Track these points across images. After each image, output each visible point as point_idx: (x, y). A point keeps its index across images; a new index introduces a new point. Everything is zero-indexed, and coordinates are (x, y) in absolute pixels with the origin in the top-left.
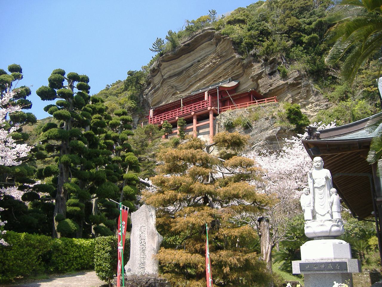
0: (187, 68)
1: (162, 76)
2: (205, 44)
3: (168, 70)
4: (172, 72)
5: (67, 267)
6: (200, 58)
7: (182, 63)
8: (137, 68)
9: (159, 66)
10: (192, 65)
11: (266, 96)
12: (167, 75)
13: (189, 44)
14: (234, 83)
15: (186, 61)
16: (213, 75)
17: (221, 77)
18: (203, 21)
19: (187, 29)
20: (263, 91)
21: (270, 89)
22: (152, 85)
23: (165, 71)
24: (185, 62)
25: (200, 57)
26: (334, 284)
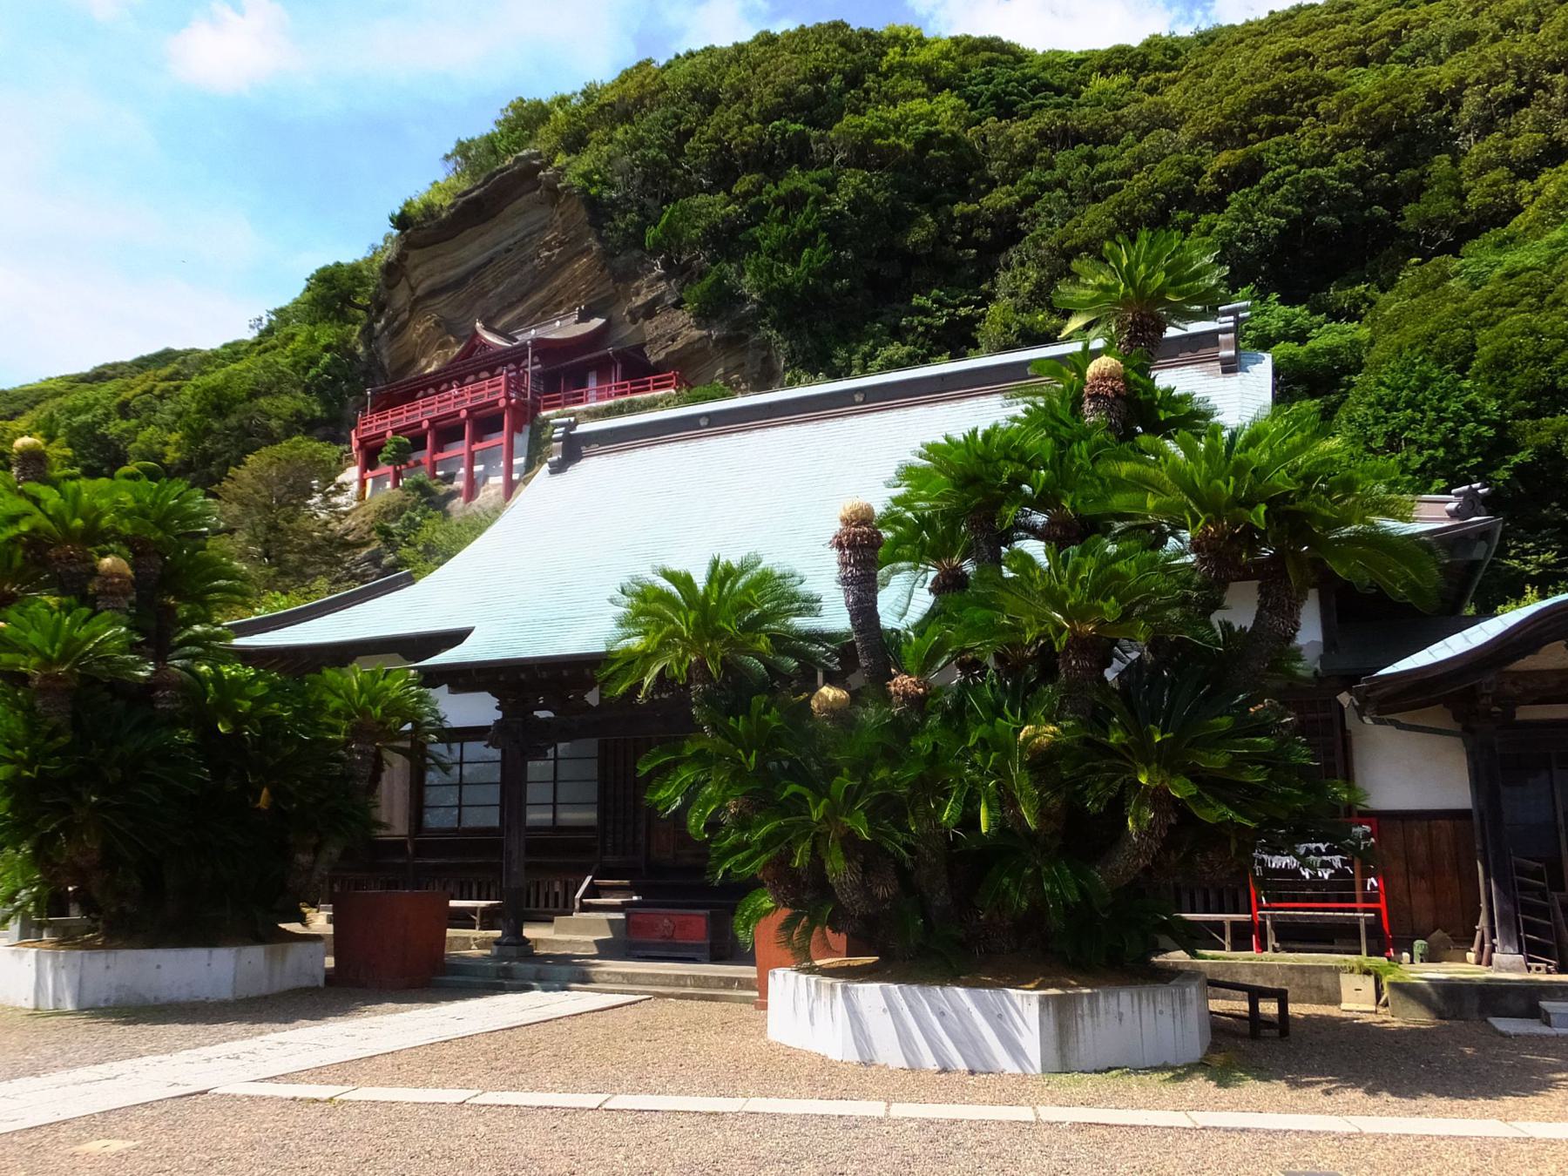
0: (479, 268)
1: (413, 289)
2: (525, 198)
3: (424, 275)
4: (437, 279)
5: (1110, 674)
6: (512, 241)
7: (464, 253)
8: (343, 261)
9: (402, 257)
10: (491, 260)
11: (658, 368)
12: (424, 285)
13: (477, 199)
14: (597, 322)
15: (475, 247)
16: (544, 293)
17: (561, 302)
18: (644, 65)
19: (584, 93)
20: (655, 356)
21: (671, 349)
22: (389, 312)
23: (417, 273)
24: (470, 251)
25: (513, 235)
26: (10, 810)
